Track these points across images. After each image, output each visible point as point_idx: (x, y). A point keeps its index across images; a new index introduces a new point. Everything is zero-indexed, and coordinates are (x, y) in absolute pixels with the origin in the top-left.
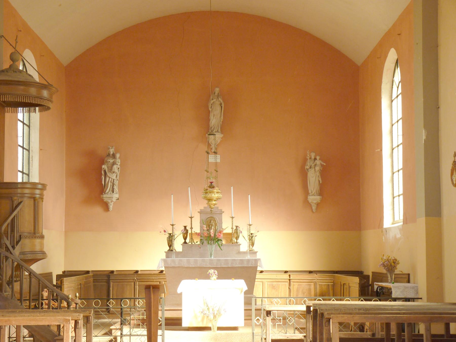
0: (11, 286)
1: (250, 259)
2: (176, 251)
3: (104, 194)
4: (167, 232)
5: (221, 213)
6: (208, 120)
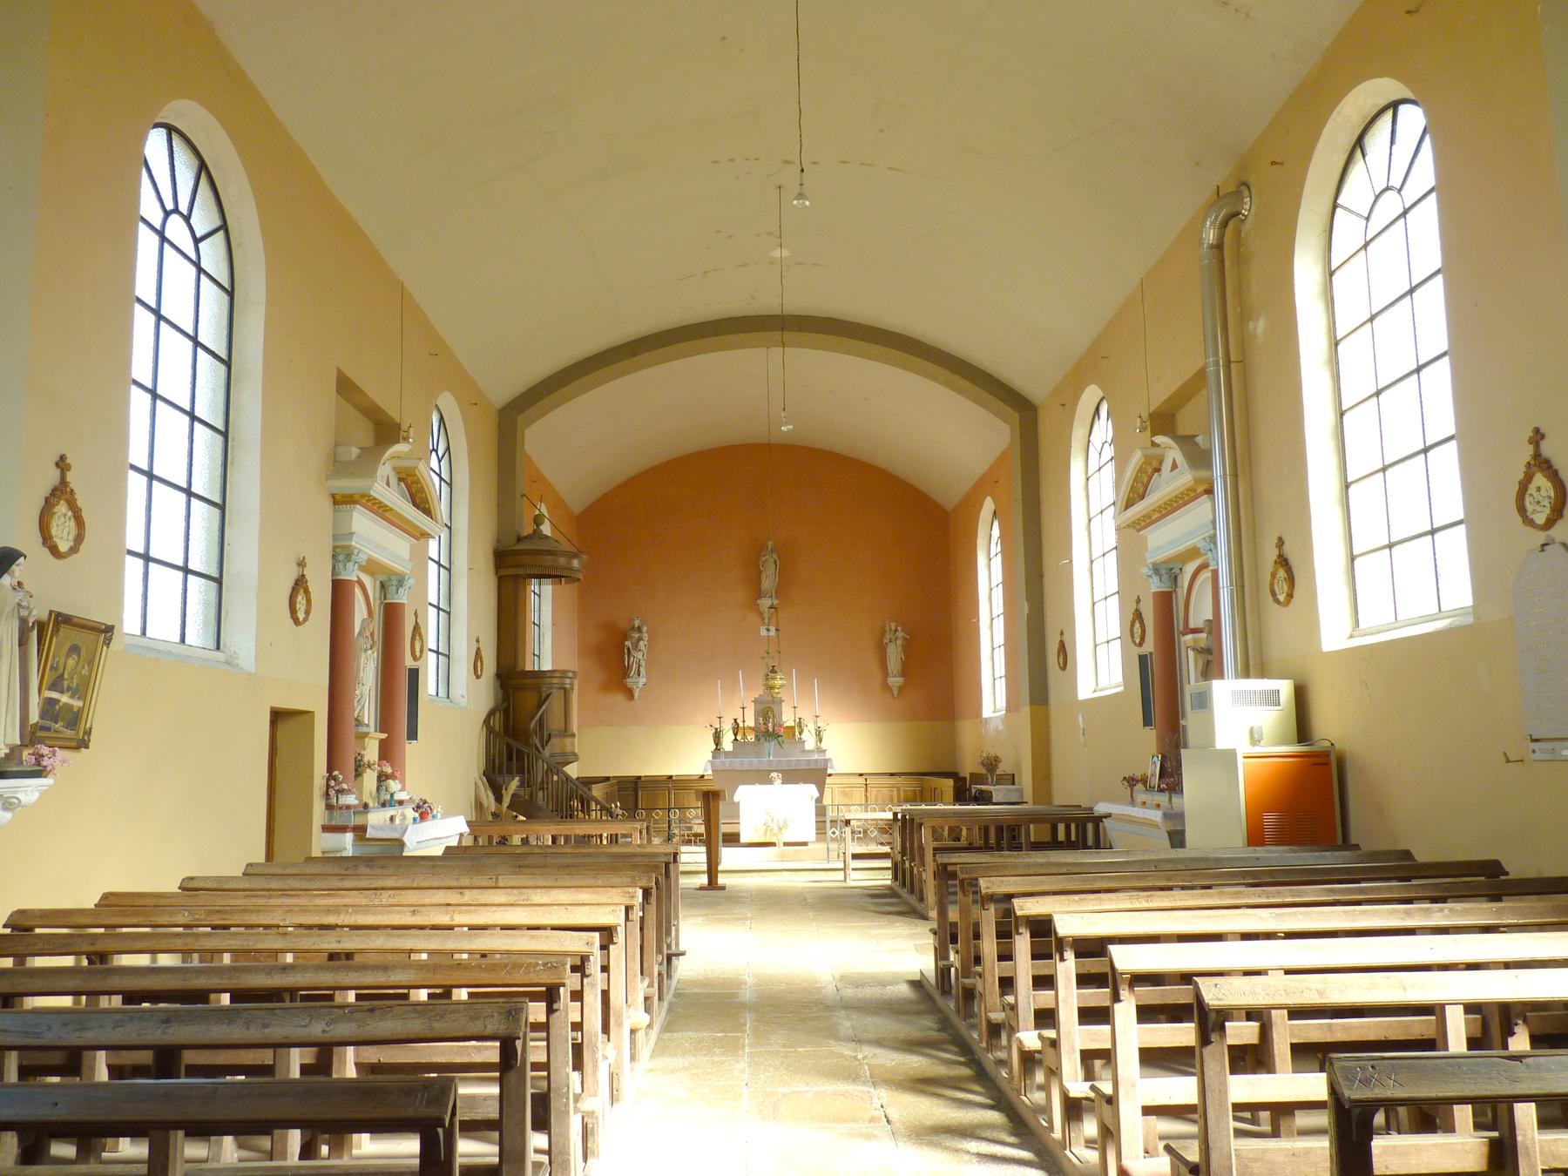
6: (759, 582)
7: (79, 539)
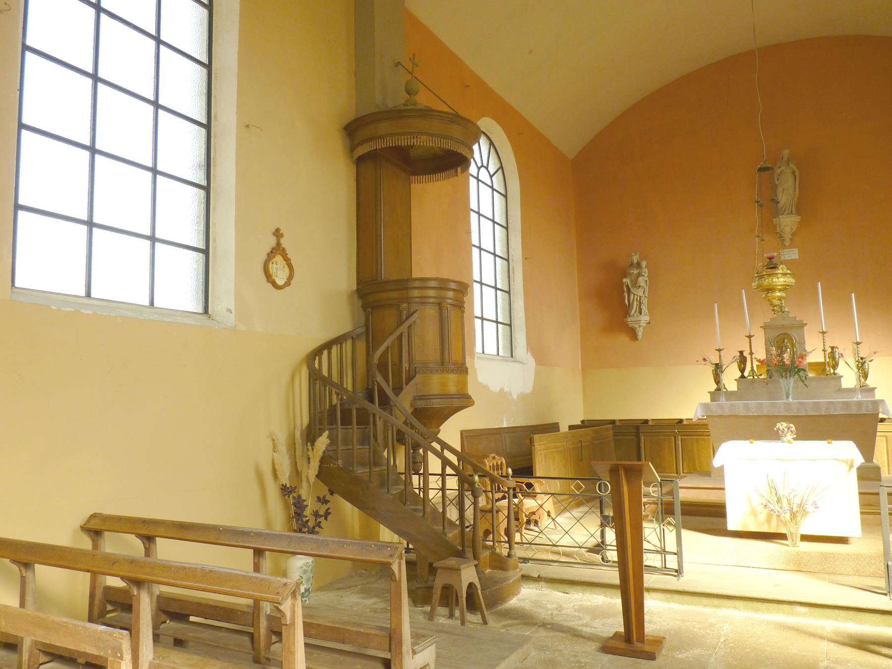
1: (863, 401)
2: (726, 389)
4: (708, 360)
5: (802, 325)
7: (290, 277)
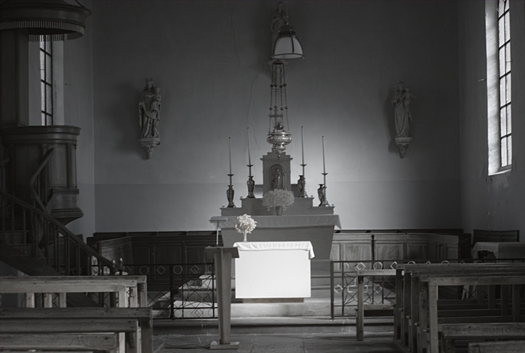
0: (43, 250)
3: (141, 137)
5: (289, 159)
